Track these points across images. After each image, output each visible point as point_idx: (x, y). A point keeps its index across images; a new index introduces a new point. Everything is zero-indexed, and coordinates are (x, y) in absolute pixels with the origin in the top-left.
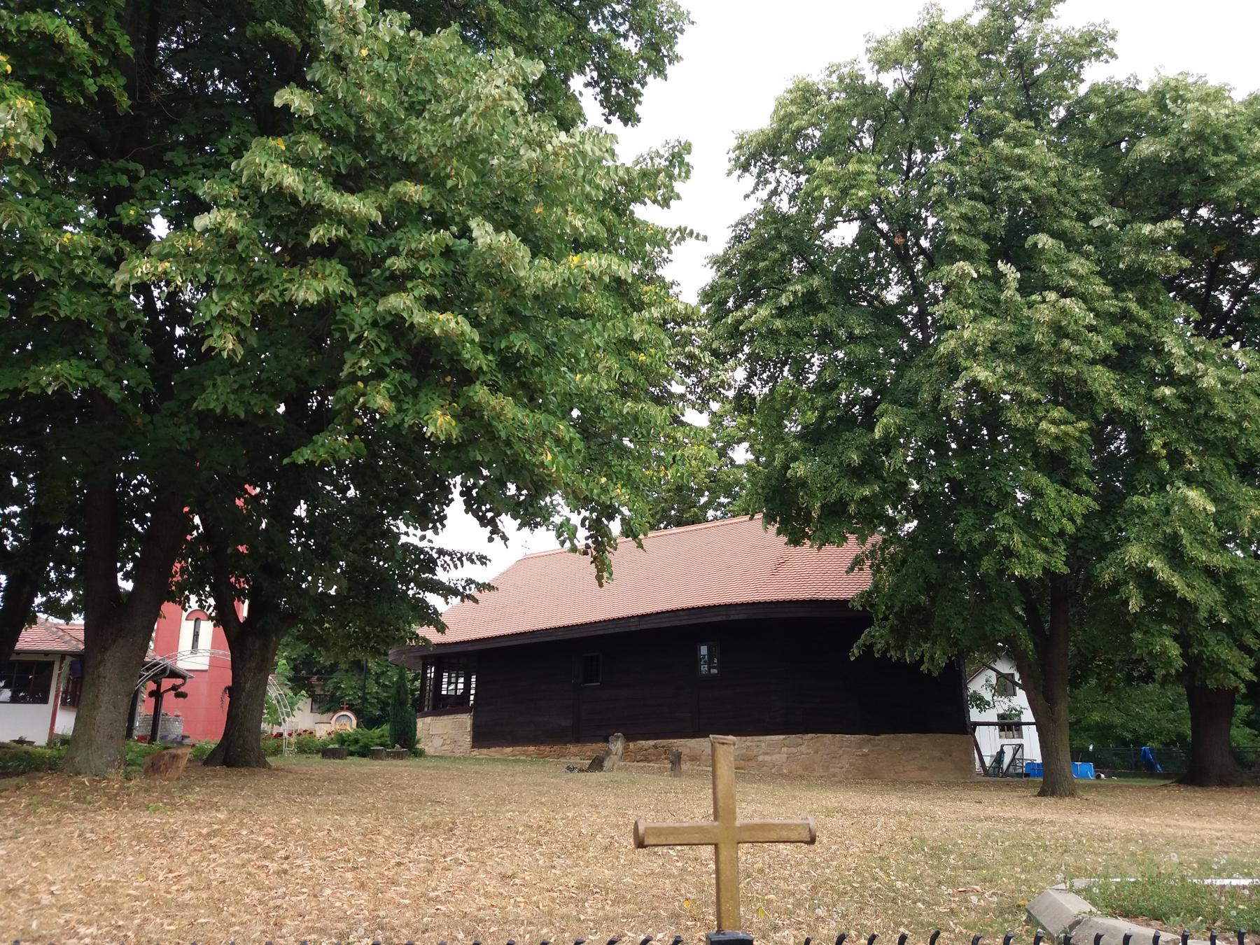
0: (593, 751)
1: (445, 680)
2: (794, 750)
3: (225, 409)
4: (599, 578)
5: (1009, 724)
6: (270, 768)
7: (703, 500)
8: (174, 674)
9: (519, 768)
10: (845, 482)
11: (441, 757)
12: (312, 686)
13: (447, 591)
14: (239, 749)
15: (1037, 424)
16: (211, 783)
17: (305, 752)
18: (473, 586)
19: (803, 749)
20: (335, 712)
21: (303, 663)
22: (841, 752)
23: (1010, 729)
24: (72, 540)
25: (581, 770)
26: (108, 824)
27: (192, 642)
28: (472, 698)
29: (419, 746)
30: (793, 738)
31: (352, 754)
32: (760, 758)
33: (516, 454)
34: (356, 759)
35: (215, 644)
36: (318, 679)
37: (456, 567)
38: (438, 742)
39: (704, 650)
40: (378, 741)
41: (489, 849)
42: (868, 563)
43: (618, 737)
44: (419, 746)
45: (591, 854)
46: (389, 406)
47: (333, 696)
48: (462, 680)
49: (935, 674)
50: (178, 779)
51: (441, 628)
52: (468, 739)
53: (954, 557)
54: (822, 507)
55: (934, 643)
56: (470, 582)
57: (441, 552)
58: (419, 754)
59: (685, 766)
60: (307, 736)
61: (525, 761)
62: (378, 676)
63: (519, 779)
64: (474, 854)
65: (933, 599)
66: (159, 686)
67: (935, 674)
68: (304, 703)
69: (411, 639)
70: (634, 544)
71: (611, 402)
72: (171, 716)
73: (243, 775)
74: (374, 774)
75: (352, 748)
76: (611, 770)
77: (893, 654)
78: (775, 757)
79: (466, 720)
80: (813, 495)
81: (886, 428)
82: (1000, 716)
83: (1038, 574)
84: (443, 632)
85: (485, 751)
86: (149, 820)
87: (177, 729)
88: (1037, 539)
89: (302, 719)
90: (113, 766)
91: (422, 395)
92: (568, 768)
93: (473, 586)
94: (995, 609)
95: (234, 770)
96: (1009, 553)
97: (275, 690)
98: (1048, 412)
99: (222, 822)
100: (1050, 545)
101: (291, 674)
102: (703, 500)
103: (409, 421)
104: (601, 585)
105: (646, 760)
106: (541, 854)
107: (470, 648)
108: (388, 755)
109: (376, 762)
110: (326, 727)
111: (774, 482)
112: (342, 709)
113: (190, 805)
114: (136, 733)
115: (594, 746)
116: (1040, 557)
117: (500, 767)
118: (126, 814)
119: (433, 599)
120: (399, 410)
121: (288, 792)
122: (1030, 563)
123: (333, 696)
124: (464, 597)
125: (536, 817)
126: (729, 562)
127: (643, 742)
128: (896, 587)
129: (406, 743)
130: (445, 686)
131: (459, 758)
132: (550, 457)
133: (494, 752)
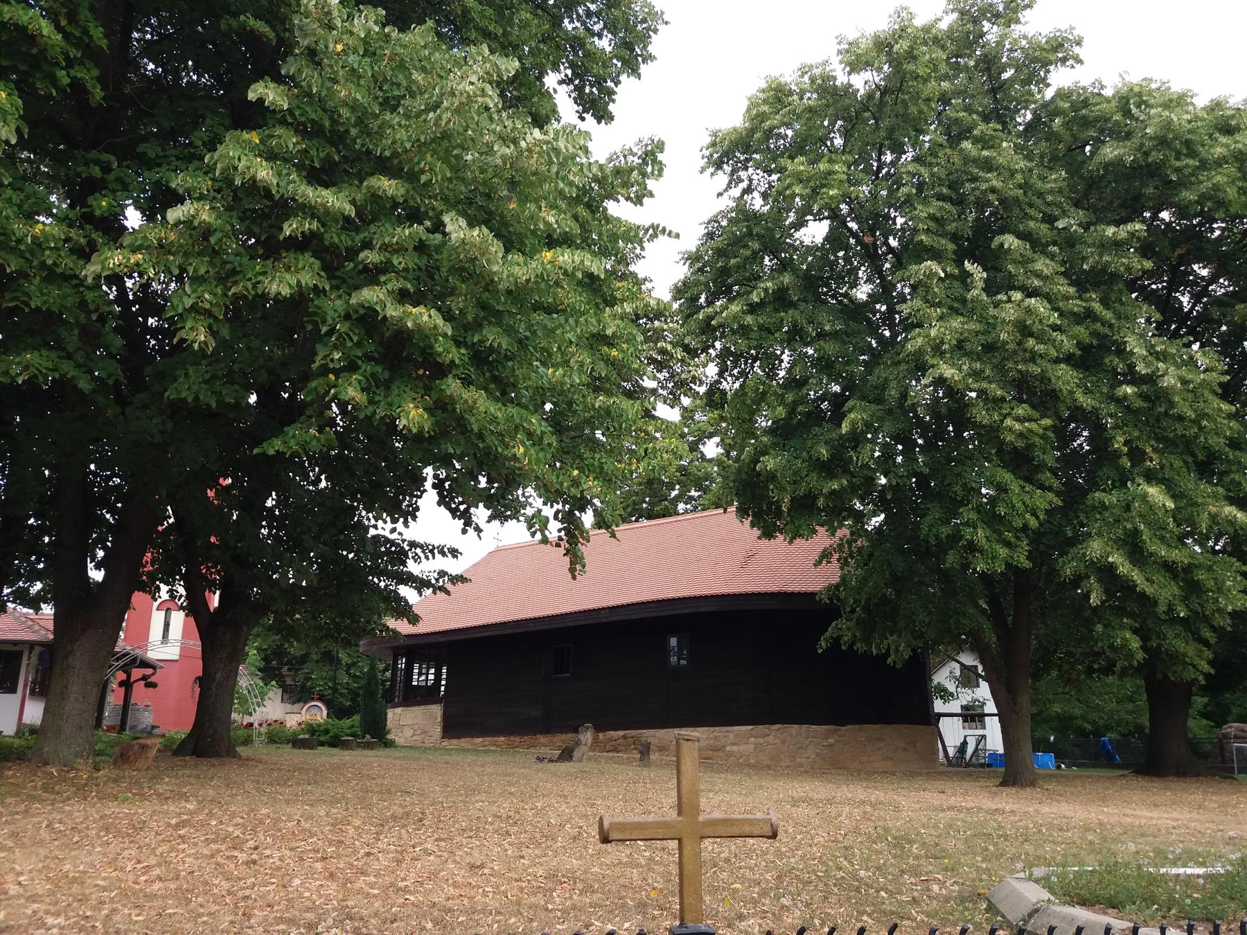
0: (563, 742)
3: (196, 399)
4: (572, 570)
5: (972, 716)
8: (145, 664)
9: (489, 759)
10: (814, 476)
11: (411, 747)
12: (283, 676)
14: (209, 740)
15: (1002, 421)
19: (770, 739)
20: (306, 702)
21: (274, 653)
23: (973, 720)
24: (42, 530)
25: (551, 761)
27: (163, 632)
28: (443, 688)
31: (322, 744)
32: (728, 748)
34: (326, 749)
35: (185, 634)
36: (289, 670)
37: (427, 558)
38: (408, 732)
39: (673, 642)
40: (349, 731)
42: (836, 556)
44: (389, 737)
47: (303, 686)
48: (432, 671)
50: (148, 769)
52: (438, 729)
54: (792, 500)
56: (442, 574)
57: (413, 544)
58: (389, 744)
60: (277, 726)
61: (495, 752)
62: (349, 666)
65: (899, 593)
66: (129, 676)
68: (275, 694)
71: (584, 396)
76: (580, 760)
77: (860, 647)
78: (742, 747)
79: (437, 710)
80: (783, 489)
81: (853, 423)
82: (963, 707)
85: (455, 741)
86: (117, 810)
88: (1000, 534)
89: (273, 709)
92: (538, 758)
96: (972, 547)
100: (1013, 540)
101: (262, 664)
102: (674, 494)
103: (381, 412)
104: (574, 578)
108: (359, 745)
109: (346, 753)
110: (295, 717)
112: (313, 699)
113: (159, 795)
115: (564, 737)
116: (1003, 552)
117: (470, 758)
118: (95, 804)
120: (371, 402)
121: (258, 782)
122: (993, 558)
123: (303, 686)
125: (505, 807)
126: (701, 554)
129: (376, 734)
130: (415, 677)
131: (429, 749)
133: (464, 743)
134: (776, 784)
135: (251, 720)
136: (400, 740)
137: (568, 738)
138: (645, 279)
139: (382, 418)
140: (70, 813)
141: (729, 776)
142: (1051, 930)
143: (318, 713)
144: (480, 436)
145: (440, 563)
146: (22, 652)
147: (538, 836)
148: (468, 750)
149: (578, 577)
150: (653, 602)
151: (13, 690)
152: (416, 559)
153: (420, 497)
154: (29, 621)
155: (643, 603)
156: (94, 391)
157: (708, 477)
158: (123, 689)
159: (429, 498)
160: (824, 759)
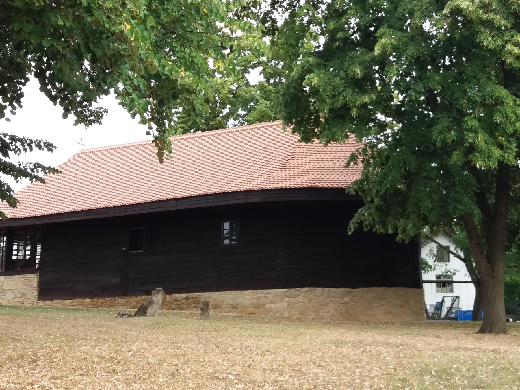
0: (137, 302)
1: (15, 248)
2: (293, 300)
4: (160, 155)
5: (444, 283)
7: (226, 111)
9: (78, 315)
10: (349, 91)
11: (14, 307)
15: (504, 47)
19: (300, 299)
22: (328, 301)
23: (444, 286)
25: (129, 316)
28: (37, 262)
30: (293, 291)
32: (268, 306)
33: (97, 22)
37: (25, 150)
38: (10, 296)
39: (227, 225)
41: (71, 377)
42: (361, 159)
43: (159, 291)
45: (162, 380)
48: (29, 248)
49: (407, 242)
51: (13, 202)
52: (35, 293)
53: (431, 152)
54: (331, 111)
55: (408, 218)
56: (37, 165)
57: (13, 138)
59: (211, 312)
61: (81, 310)
63: (82, 322)
64: (58, 381)
65: (409, 186)
67: (407, 242)
76: (153, 315)
77: (379, 229)
78: (279, 305)
79: (33, 279)
80: (323, 101)
81: (384, 47)
82: (438, 277)
83: (494, 165)
85: (49, 302)
88: (495, 138)
92: (119, 315)
94: (457, 193)
96: (472, 149)
98: (512, 36)
100: (505, 143)
102: (226, 111)
104: (161, 161)
105: (179, 308)
106: (118, 380)
107: (37, 223)
111: (292, 90)
115: (138, 298)
116: (497, 152)
117: (63, 314)
122: (489, 157)
124: (32, 177)
125: (106, 350)
126: (254, 156)
127: (177, 295)
128: (385, 176)
130: (15, 253)
131: (28, 308)
132: (128, 27)
133: (57, 303)
134: (311, 331)
137: (142, 299)
141: (273, 326)
142: (1, 366)
144: (89, 10)
145: (37, 156)
147: (141, 373)
148: (60, 309)
149: (165, 160)
152: (16, 150)
153: (24, 84)
157: (253, 99)
160: (341, 314)
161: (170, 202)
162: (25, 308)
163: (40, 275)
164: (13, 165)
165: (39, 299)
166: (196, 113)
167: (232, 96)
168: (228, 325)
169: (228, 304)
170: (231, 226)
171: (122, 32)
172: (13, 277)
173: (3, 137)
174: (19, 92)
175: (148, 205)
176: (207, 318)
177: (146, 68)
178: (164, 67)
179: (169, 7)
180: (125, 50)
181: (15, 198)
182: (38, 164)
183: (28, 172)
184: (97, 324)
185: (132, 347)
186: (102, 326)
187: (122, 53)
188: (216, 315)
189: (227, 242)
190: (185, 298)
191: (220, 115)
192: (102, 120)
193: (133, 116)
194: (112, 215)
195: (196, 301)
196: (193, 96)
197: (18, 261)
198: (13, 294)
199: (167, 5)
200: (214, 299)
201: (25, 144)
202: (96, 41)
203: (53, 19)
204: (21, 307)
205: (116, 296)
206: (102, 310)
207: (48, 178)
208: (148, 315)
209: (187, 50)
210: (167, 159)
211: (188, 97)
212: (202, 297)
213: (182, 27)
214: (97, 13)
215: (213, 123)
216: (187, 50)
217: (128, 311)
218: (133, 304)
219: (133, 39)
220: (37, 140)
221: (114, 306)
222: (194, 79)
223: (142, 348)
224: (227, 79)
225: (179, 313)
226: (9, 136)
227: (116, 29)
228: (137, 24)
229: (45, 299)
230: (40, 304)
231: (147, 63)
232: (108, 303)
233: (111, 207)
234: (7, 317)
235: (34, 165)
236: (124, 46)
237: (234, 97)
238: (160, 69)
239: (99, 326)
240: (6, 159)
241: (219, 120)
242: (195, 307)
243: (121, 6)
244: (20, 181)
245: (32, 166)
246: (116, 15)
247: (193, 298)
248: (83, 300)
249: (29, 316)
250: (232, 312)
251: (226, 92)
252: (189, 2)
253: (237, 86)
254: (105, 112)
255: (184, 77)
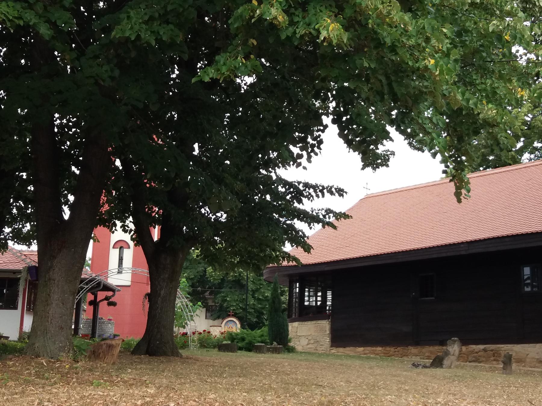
0: (431, 352)
1: (306, 294)
3: (138, 37)
4: (458, 195)
6: (181, 357)
7: (520, 145)
8: (107, 288)
9: (373, 363)
11: (309, 353)
12: (206, 299)
13: (310, 218)
14: (157, 343)
16: (139, 367)
17: (205, 347)
18: (331, 215)
20: (223, 319)
21: (198, 282)
24: (28, 182)
25: (425, 367)
26: (61, 395)
27: (117, 258)
29: (291, 344)
31: (240, 349)
34: (244, 353)
35: (135, 263)
36: (210, 294)
37: (318, 196)
38: (304, 342)
39: (527, 271)
40: (259, 339)
43: (455, 341)
44: (291, 344)
46: (282, 18)
47: (221, 306)
50: (114, 363)
51: (307, 248)
52: (328, 340)
56: (329, 211)
57: (307, 185)
58: (291, 350)
59: (514, 366)
60: (206, 334)
62: (254, 292)
63: (378, 371)
66: (96, 297)
68: (200, 313)
69: (283, 258)
70: (454, 190)
71: (475, 23)
72: (105, 319)
73: (162, 362)
74: (262, 363)
75: (240, 345)
76: (450, 367)
79: (325, 325)
84: (309, 252)
85: (341, 350)
86: (93, 393)
87: (110, 329)
89: (197, 323)
90: (64, 351)
91: (310, 8)
92: (414, 365)
93: (331, 215)
95: (155, 359)
97: (181, 300)
99: (152, 396)
101: (191, 290)
102: (520, 145)
103: (301, 31)
104: (459, 201)
105: (477, 360)
107: (327, 268)
108: (268, 350)
109: (260, 355)
110: (218, 330)
112: (229, 316)
113: (125, 382)
114: (81, 332)
115: (431, 348)
117: (358, 362)
118: (75, 388)
119: (299, 225)
120: (292, 23)
121: (200, 375)
123: (221, 306)
124: (326, 224)
127: (474, 347)
129: (280, 341)
130: (306, 298)
132: (432, 61)
133: (349, 351)
135: (185, 331)
136: (299, 348)
137: (436, 350)
138: (320, 149)
139: (302, 37)
140: (57, 394)
143: (233, 326)
144: (393, 49)
146: (19, 279)
148: (353, 357)
150: (508, 236)
151: (16, 308)
152: (309, 197)
153: (323, 131)
154: (22, 254)
155: (498, 238)
156: (53, 38)
158: (92, 307)
159: (331, 134)
161: (462, 246)
162: (320, 355)
163: (331, 322)
164: (306, 211)
165: (331, 346)
166: (500, 148)
167: (526, 128)
168: (536, 381)
169: (533, 358)
170: (532, 271)
171: (426, 67)
172: (306, 323)
173: (296, 184)
174: (319, 139)
175: (413, 252)
176: (511, 373)
177: (448, 104)
178: (468, 101)
179: (467, 38)
180: (426, 87)
181: (308, 244)
182: (329, 209)
183: (321, 219)
184: (394, 373)
185: (439, 400)
186: (399, 376)
187: (425, 90)
188: (520, 370)
189: (528, 289)
190: (483, 349)
191: (513, 149)
192: (389, 163)
193: (434, 155)
194: (400, 260)
195: (496, 354)
196: (496, 129)
197: (309, 306)
198: (307, 340)
199: (465, 37)
200: (516, 352)
201: (318, 191)
202: (399, 80)
203: (358, 62)
204: (315, 353)
205: (409, 345)
206: (395, 360)
207: (341, 224)
208: (444, 366)
209: (489, 82)
210: (466, 198)
211: (491, 131)
212: (502, 349)
213: (482, 57)
214: (400, 51)
215: (504, 158)
216: (489, 82)
217: (423, 362)
218: (427, 354)
219: (437, 73)
220: (328, 186)
221: (407, 356)
222: (497, 112)
223: (450, 401)
224: (520, 110)
225: (478, 366)
226: (303, 183)
227: (421, 64)
228: (440, 58)
229: (337, 347)
230: (333, 351)
231: (450, 98)
232: (401, 352)
233: (399, 252)
234: (306, 363)
235: (326, 211)
236: (426, 84)
237: (529, 129)
238: (464, 103)
239: (395, 376)
240: (300, 206)
241: (512, 155)
242: (494, 360)
243: (425, 42)
244: (313, 227)
245: (323, 212)
246: (419, 51)
247: (492, 351)
248: (374, 348)
249: (325, 362)
250: (538, 367)
251: (520, 124)
252: (490, 31)
253: (531, 116)
254: (391, 154)
255: (489, 111)
